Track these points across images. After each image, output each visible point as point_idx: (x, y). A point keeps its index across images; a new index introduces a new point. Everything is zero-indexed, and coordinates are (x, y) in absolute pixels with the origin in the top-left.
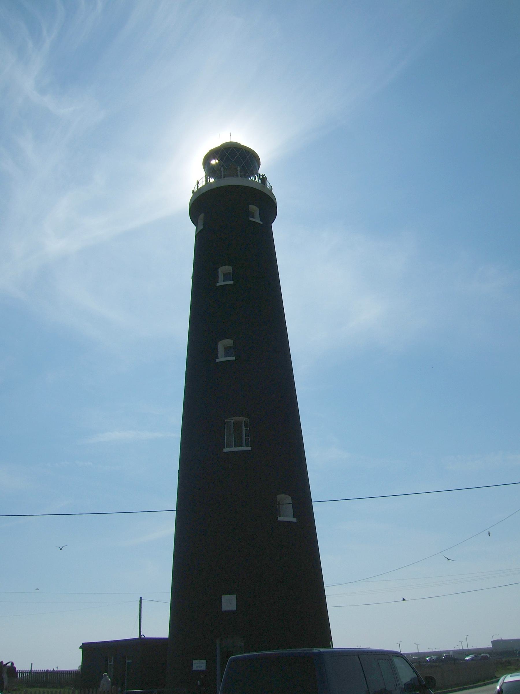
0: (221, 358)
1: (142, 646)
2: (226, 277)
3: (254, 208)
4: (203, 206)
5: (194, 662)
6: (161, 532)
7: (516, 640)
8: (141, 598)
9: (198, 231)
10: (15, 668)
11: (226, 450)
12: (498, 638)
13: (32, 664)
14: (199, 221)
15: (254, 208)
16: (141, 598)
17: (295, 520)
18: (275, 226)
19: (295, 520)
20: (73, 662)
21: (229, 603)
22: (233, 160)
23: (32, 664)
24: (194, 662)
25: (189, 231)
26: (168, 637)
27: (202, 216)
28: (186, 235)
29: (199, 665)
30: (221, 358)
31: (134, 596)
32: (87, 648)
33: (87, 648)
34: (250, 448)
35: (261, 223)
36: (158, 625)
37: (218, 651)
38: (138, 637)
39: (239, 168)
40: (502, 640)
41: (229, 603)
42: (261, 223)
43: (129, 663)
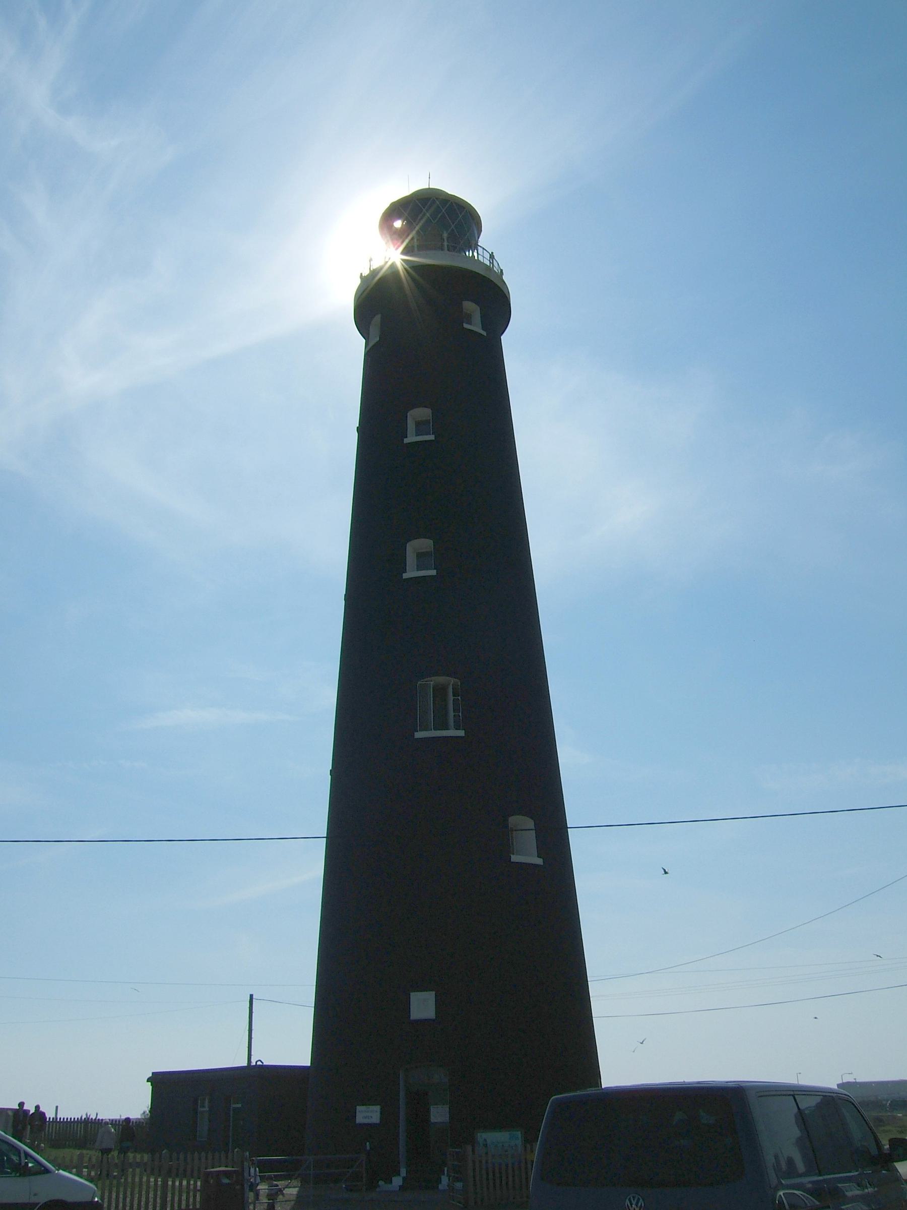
0: (411, 573)
1: (258, 1079)
2: (420, 427)
3: (469, 306)
4: (376, 304)
5: (359, 1108)
6: (304, 872)
7: (888, 1082)
8: (251, 996)
9: (371, 344)
10: (44, 1114)
11: (419, 735)
12: (850, 1079)
13: (57, 1107)
14: (371, 329)
15: (469, 306)
16: (251, 996)
17: (539, 861)
18: (507, 339)
19: (539, 861)
20: (136, 1104)
21: (423, 1005)
22: (436, 219)
23: (57, 1107)
24: (359, 1108)
25: (355, 346)
26: (309, 1065)
27: (377, 319)
28: (347, 356)
29: (368, 1114)
30: (411, 573)
31: (249, 989)
32: (159, 1081)
33: (159, 1081)
34: (461, 733)
35: (484, 333)
36: (288, 1040)
37: (402, 1094)
38: (246, 1064)
39: (445, 235)
40: (855, 1084)
41: (423, 1005)
42: (484, 333)
43: (235, 1109)
